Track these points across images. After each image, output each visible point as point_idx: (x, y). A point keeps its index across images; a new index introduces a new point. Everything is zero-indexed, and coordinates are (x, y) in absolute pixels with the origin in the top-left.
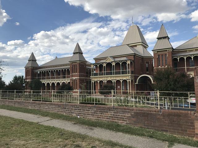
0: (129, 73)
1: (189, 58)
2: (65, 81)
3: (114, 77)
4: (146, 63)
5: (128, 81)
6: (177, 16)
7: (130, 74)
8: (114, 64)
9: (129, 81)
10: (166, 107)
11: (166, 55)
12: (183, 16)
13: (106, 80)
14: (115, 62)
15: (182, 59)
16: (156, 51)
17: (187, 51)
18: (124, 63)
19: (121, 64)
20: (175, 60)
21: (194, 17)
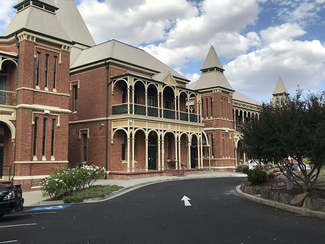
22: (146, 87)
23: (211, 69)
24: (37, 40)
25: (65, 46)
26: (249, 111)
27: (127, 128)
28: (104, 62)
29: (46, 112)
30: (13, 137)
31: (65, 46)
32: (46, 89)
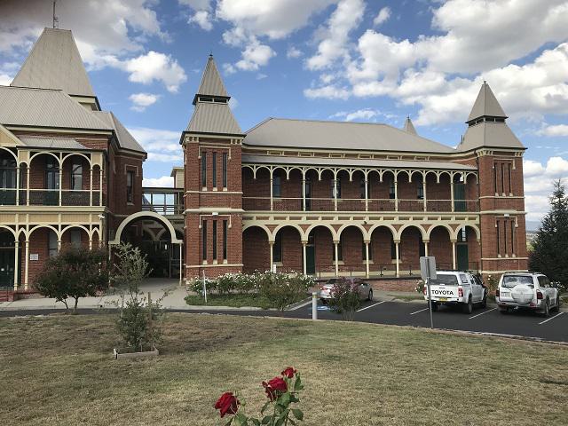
0: (96, 203)
1: (279, 173)
2: (421, 222)
3: (22, 213)
4: (128, 172)
5: (91, 233)
6: (97, 54)
7: (101, 208)
8: (24, 158)
9: (96, 233)
10: (15, 356)
11: (225, 154)
12: (111, 60)
13: (31, 227)
14: (32, 154)
15: (263, 173)
16: (491, 150)
17: (266, 152)
18: (77, 160)
19: (61, 161)
20: (247, 172)
21: (136, 71)
23: (479, 120)
25: (234, 140)
27: (13, 227)
29: (214, 214)
30: (479, 237)
31: (234, 140)
32: (504, 194)
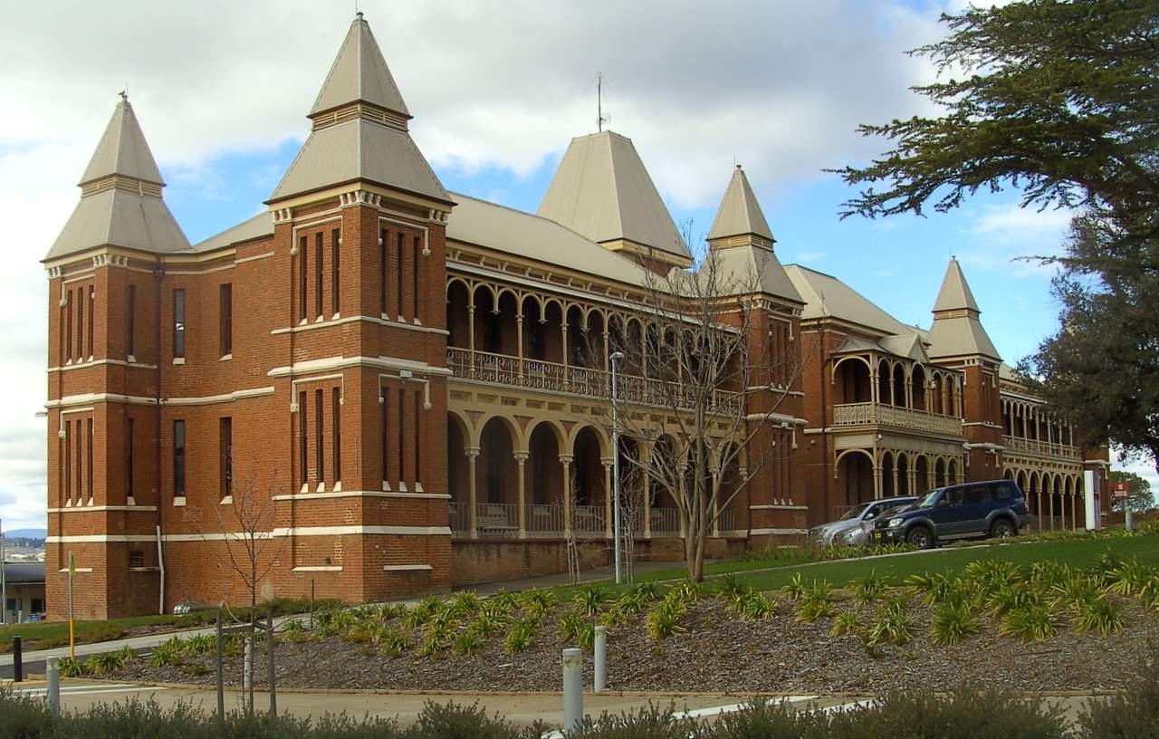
22: (472, 291)
24: (385, 202)
26: (1008, 399)
28: (815, 323)
